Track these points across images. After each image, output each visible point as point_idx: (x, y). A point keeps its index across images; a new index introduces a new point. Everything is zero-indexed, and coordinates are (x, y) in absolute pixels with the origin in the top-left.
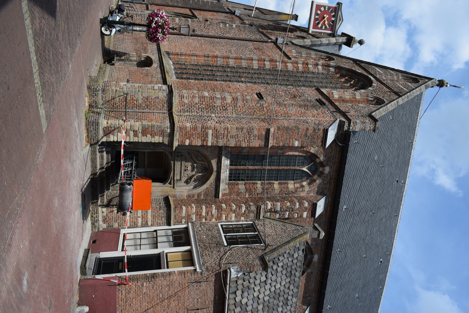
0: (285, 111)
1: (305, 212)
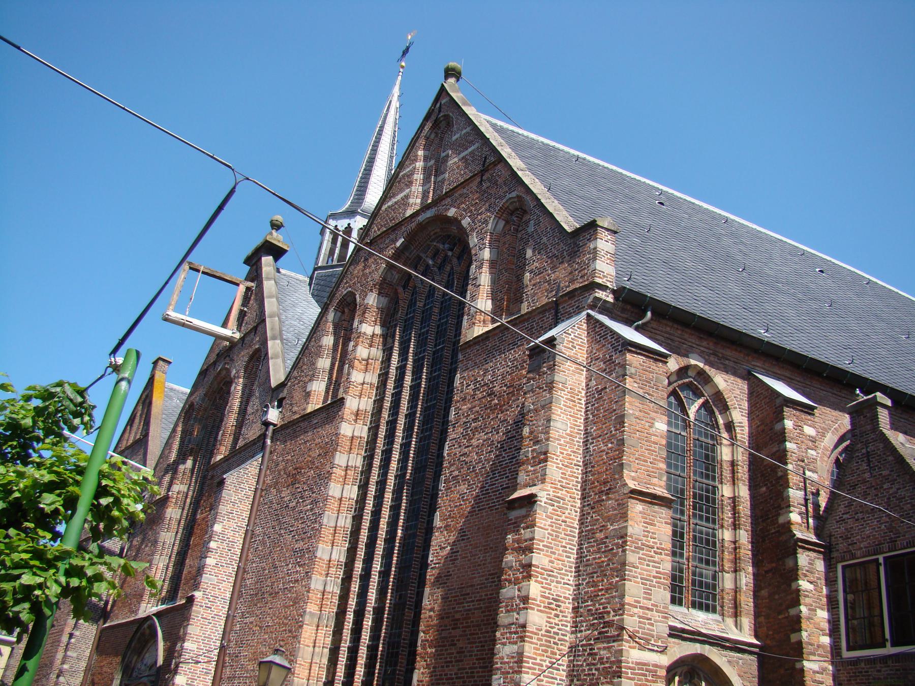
0: (568, 443)
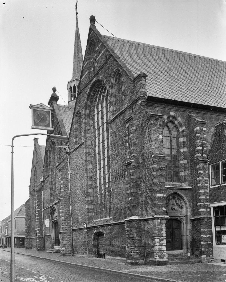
1: (203, 129)
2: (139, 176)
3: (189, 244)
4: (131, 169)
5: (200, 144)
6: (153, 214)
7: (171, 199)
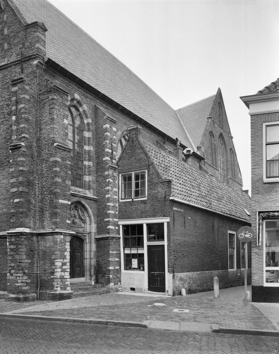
2: (32, 169)
3: (93, 270)
4: (19, 156)
5: (109, 146)
6: (53, 226)
7: (73, 209)
